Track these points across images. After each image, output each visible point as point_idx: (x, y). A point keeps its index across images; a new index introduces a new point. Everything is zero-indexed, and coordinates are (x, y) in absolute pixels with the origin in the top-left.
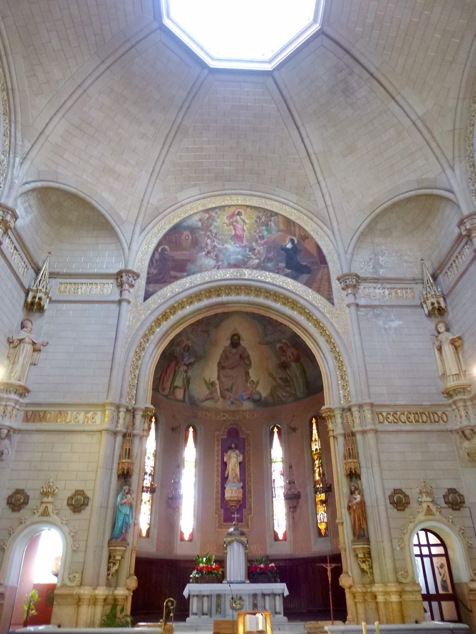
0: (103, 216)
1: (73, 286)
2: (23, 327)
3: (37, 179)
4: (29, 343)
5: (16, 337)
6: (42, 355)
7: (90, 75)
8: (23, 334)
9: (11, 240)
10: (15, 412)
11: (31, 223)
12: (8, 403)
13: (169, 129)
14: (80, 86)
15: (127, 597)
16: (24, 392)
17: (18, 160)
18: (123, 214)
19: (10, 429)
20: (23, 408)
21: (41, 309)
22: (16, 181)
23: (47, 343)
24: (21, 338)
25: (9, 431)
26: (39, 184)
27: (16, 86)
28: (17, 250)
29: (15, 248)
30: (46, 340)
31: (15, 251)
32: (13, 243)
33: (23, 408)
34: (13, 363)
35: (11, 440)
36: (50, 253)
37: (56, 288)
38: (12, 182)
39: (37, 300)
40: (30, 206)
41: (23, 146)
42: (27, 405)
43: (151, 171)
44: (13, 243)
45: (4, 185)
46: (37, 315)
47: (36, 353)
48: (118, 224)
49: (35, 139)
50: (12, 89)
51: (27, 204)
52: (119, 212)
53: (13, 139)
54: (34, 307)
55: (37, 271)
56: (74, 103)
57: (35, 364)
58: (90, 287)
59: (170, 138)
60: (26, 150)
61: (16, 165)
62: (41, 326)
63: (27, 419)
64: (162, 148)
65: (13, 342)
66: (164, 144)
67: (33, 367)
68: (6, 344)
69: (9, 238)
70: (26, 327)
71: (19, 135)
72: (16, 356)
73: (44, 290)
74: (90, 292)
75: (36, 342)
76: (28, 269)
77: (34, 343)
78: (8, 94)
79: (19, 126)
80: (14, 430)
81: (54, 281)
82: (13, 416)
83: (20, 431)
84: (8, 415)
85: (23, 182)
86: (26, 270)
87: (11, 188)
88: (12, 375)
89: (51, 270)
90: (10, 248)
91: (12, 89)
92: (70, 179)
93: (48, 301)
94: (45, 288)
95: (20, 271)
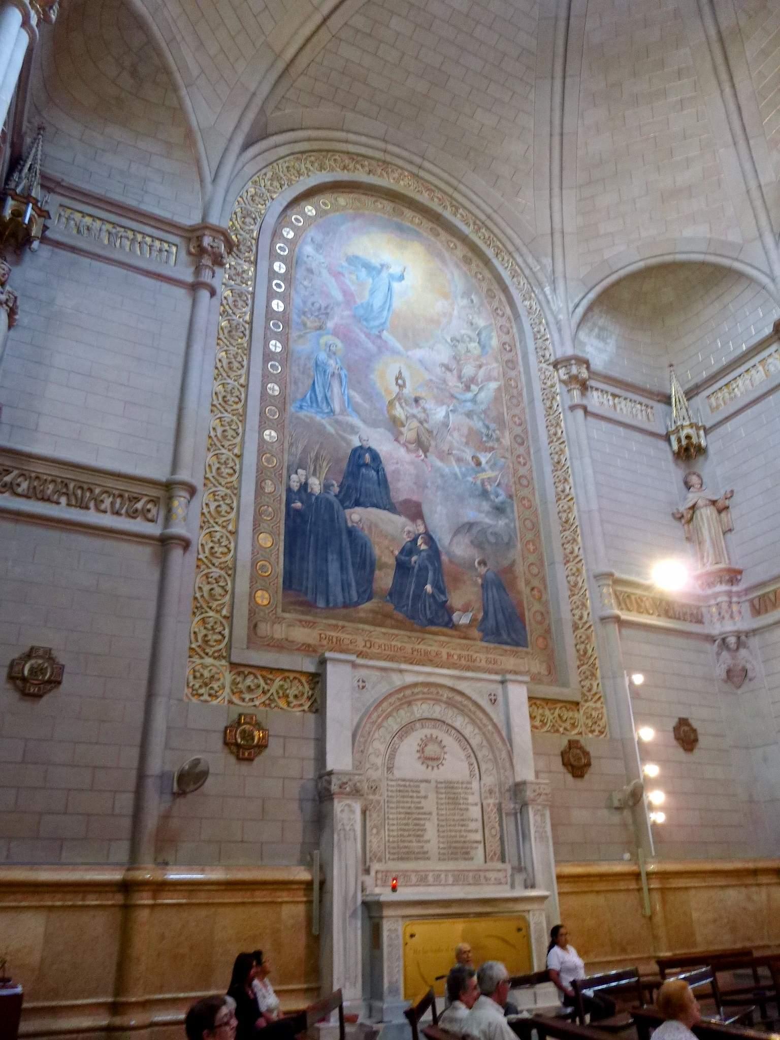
0: (703, 264)
1: (726, 390)
2: (688, 486)
3: (586, 290)
4: (706, 506)
5: (683, 508)
6: (734, 513)
7: (551, 110)
8: (692, 497)
9: (602, 391)
10: (735, 608)
11: (618, 347)
12: (719, 599)
13: (709, 58)
14: (551, 135)
15: (695, 944)
16: (732, 575)
17: (547, 289)
18: (734, 236)
19: (738, 635)
20: (744, 599)
21: (701, 450)
22: (561, 317)
23: (732, 492)
24: (690, 504)
25: (739, 638)
26: (592, 296)
27: (489, 211)
28: (619, 397)
29: (614, 396)
30: (728, 489)
31: (617, 400)
32: (607, 392)
33: (744, 599)
34: (700, 543)
35: (748, 648)
36: (671, 365)
37: (704, 409)
38: (558, 322)
39: (684, 442)
40: (602, 329)
41: (543, 268)
42: (747, 591)
43: (730, 141)
44: (607, 392)
45: (550, 334)
46: (701, 459)
47: (723, 515)
48: (735, 255)
49: (550, 247)
50: (489, 217)
51: (596, 330)
52: (723, 238)
53: (527, 272)
54: (689, 453)
55: (666, 400)
56: (561, 160)
57: (730, 530)
58: (747, 376)
59: (722, 69)
60: (549, 269)
61: (550, 297)
62: (714, 470)
63: (758, 609)
64: (722, 91)
65: (683, 516)
66: (719, 84)
67: (729, 535)
68: (676, 523)
69: (597, 389)
70: (693, 486)
71: (530, 260)
72: (698, 530)
73: (687, 423)
74: (752, 385)
75: (715, 498)
76: (652, 408)
77: (714, 502)
78: (487, 228)
79: (524, 250)
80: (747, 634)
81: (698, 400)
82: (736, 614)
83: (755, 631)
84: (727, 616)
85: (571, 309)
86: (649, 410)
87: (560, 330)
88: (705, 560)
89: (687, 386)
90: (605, 402)
91: (489, 217)
92: (626, 254)
93: (702, 432)
94: (687, 418)
95: (640, 420)
